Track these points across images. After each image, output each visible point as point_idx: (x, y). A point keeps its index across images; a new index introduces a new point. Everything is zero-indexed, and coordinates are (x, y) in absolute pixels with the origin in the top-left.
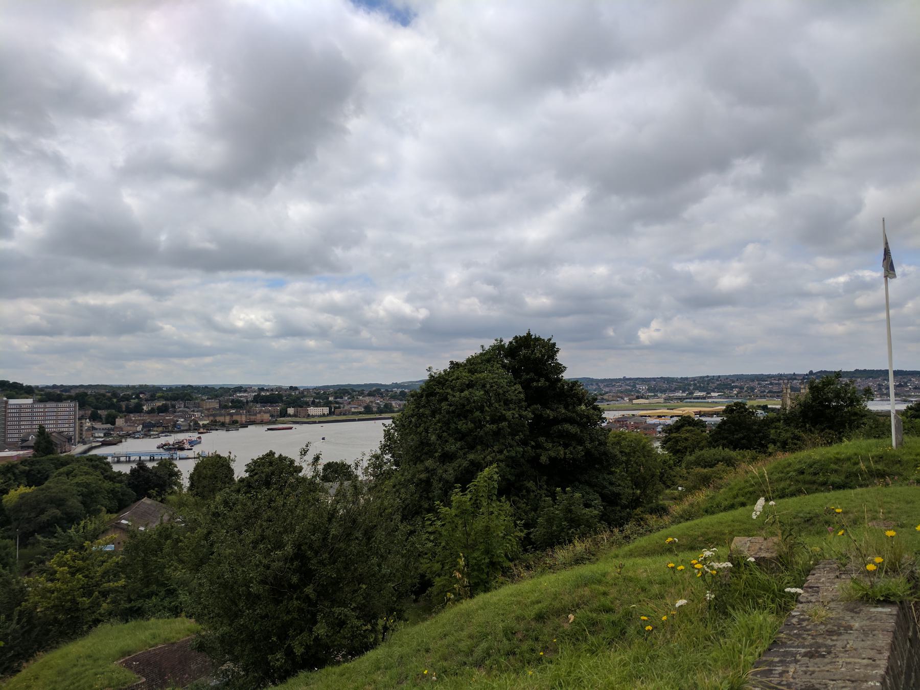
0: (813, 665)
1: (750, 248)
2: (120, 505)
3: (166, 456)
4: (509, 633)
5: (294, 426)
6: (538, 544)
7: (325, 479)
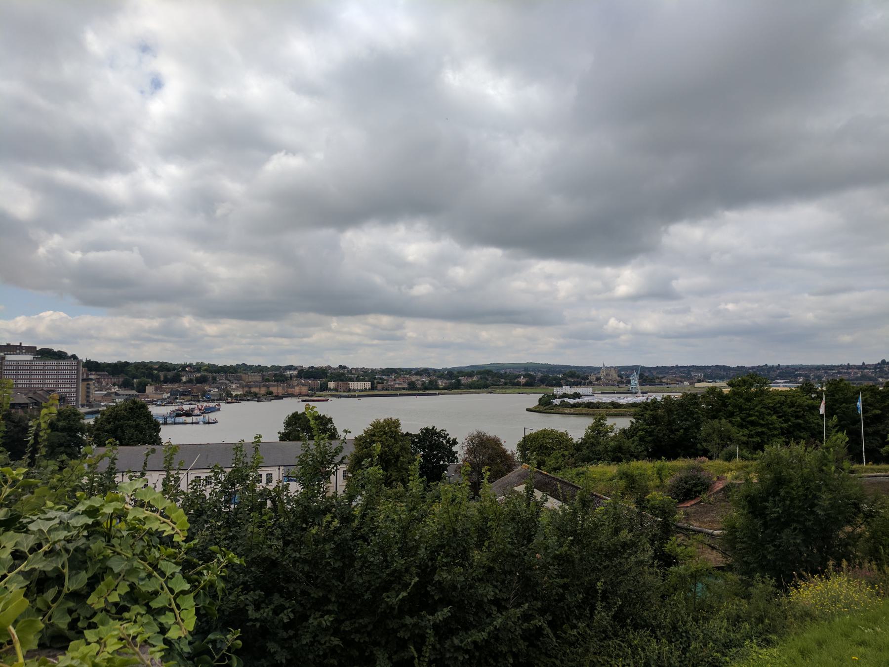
5: (330, 399)
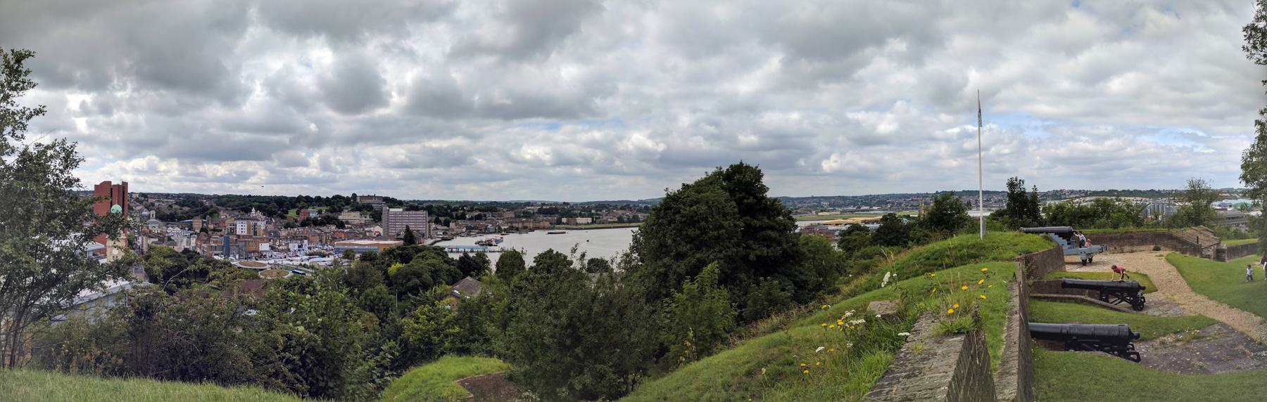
0: (910, 383)
1: (899, 104)
2: (454, 281)
3: (481, 249)
4: (726, 386)
6: (746, 319)
7: (589, 270)
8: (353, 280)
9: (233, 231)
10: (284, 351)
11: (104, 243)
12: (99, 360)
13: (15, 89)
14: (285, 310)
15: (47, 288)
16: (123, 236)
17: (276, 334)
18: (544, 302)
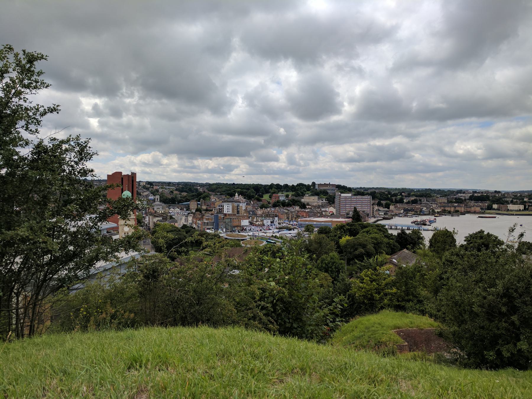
2: (392, 251)
3: (416, 227)
8: (312, 248)
9: (221, 211)
10: (260, 300)
11: (117, 222)
12: (113, 317)
13: (28, 87)
14: (261, 270)
15: (66, 263)
16: (133, 216)
17: (254, 288)
18: (473, 276)
